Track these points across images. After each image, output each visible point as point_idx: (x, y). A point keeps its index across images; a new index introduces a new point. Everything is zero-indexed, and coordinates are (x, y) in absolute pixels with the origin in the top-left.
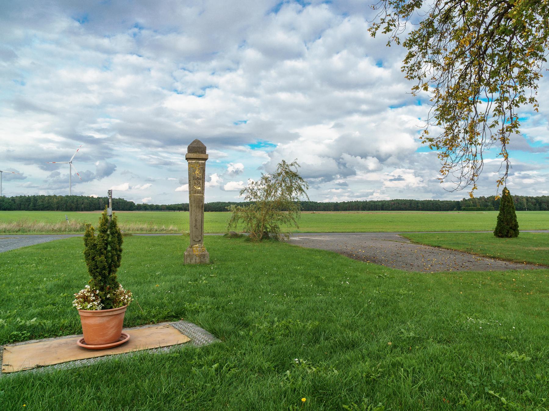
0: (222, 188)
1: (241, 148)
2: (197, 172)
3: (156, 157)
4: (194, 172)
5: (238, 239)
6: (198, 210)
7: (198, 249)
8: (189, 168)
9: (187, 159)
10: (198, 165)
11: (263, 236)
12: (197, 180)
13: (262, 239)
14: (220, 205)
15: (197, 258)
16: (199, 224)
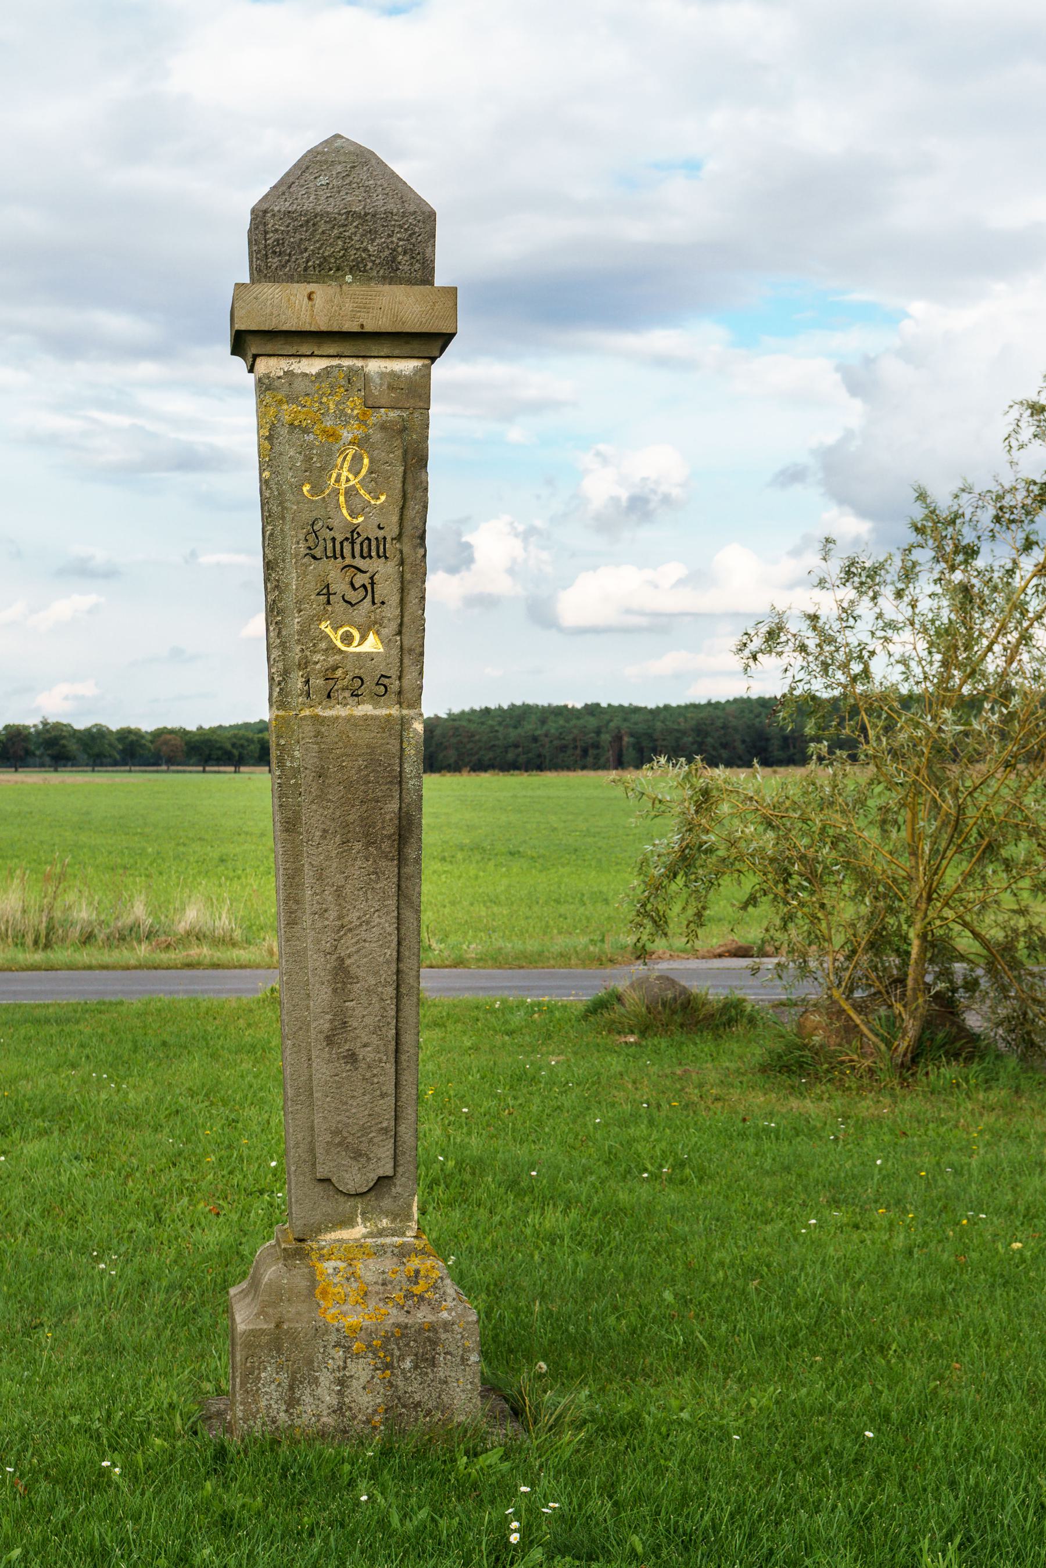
0: (541, 614)
1: (660, 339)
2: (344, 476)
3: (124, 421)
4: (317, 470)
5: (702, 1046)
6: (358, 869)
7: (369, 1270)
8: (269, 438)
9: (241, 342)
10: (354, 406)
11: (928, 1024)
12: (348, 546)
13: (916, 1055)
14: (530, 726)
15: (361, 1370)
16: (367, 1014)
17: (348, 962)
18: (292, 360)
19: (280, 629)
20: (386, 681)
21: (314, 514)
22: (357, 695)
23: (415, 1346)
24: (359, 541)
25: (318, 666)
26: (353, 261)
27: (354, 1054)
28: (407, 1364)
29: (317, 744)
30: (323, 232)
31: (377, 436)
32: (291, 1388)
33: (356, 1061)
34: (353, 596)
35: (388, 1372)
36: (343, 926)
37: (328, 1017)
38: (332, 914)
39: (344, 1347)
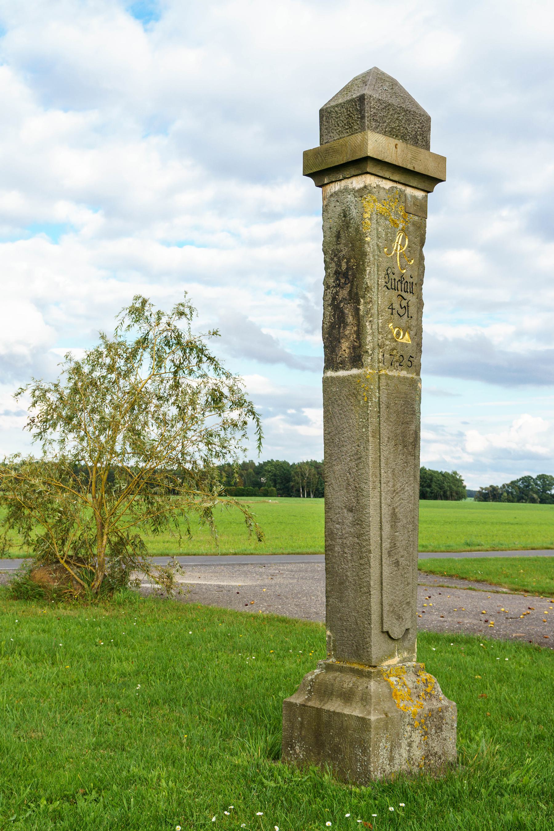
17: (397, 510)
18: (380, 179)
19: (372, 325)
20: (411, 359)
21: (388, 264)
22: (401, 366)
23: (433, 721)
24: (403, 282)
25: (388, 347)
26: (402, 133)
27: (398, 561)
28: (433, 731)
29: (387, 390)
30: (392, 115)
31: (411, 228)
32: (391, 751)
33: (399, 565)
34: (402, 312)
35: (426, 736)
36: (395, 491)
37: (389, 541)
38: (391, 484)
39: (411, 725)
